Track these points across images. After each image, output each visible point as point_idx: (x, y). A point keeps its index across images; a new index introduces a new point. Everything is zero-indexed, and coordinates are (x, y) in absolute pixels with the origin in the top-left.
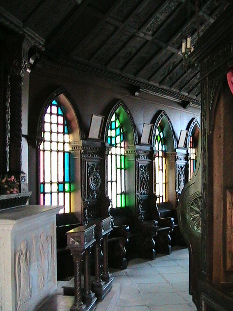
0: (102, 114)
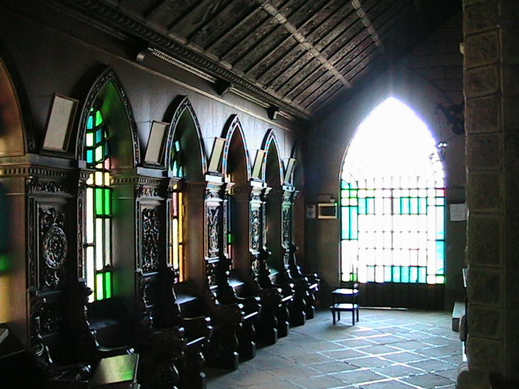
0: (71, 96)
